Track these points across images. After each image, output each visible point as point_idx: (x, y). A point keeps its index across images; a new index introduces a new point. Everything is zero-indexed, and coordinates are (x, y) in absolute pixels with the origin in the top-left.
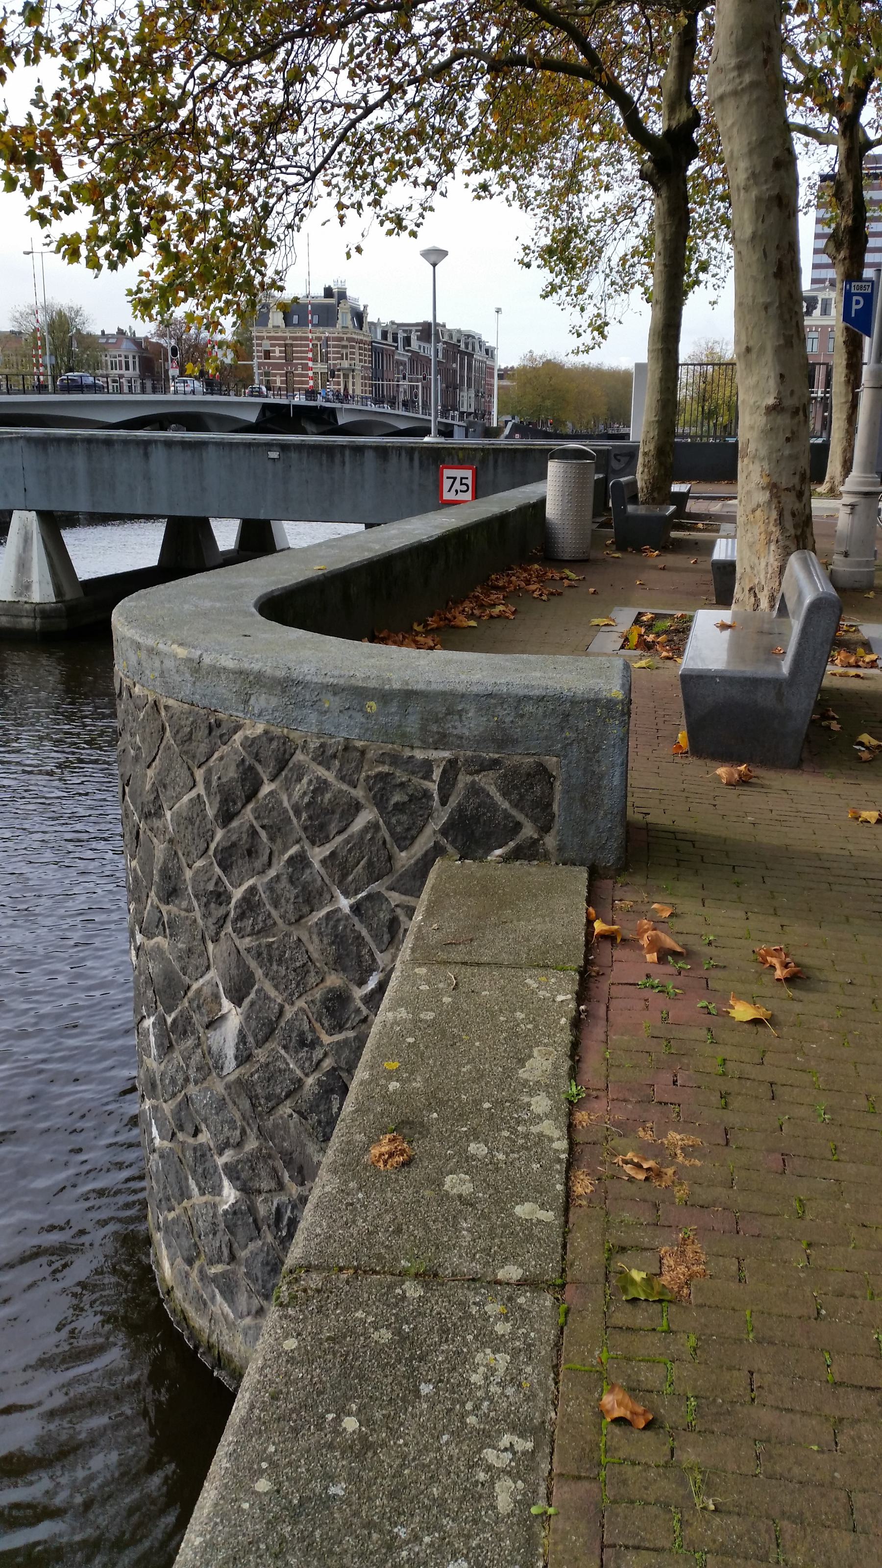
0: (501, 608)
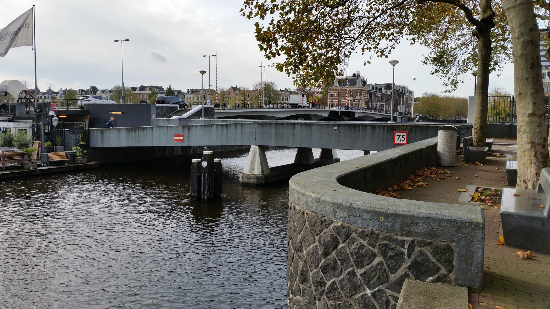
0: (421, 183)
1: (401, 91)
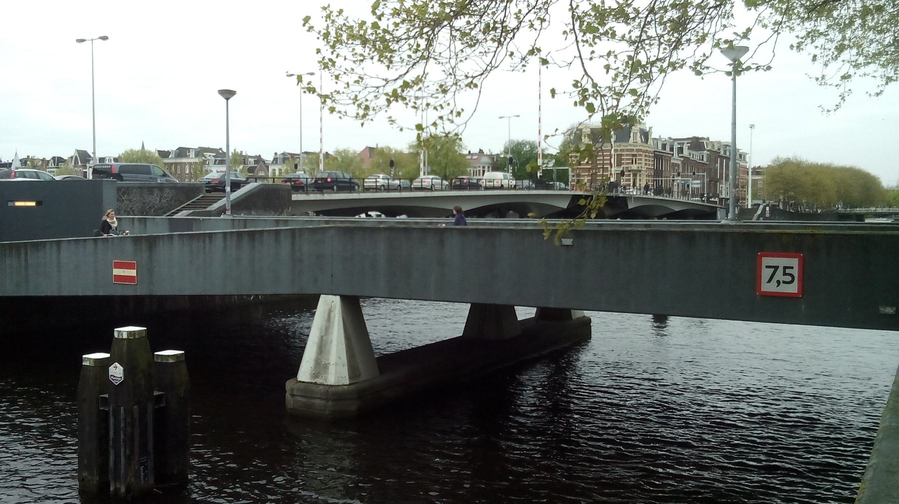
1: (722, 153)
